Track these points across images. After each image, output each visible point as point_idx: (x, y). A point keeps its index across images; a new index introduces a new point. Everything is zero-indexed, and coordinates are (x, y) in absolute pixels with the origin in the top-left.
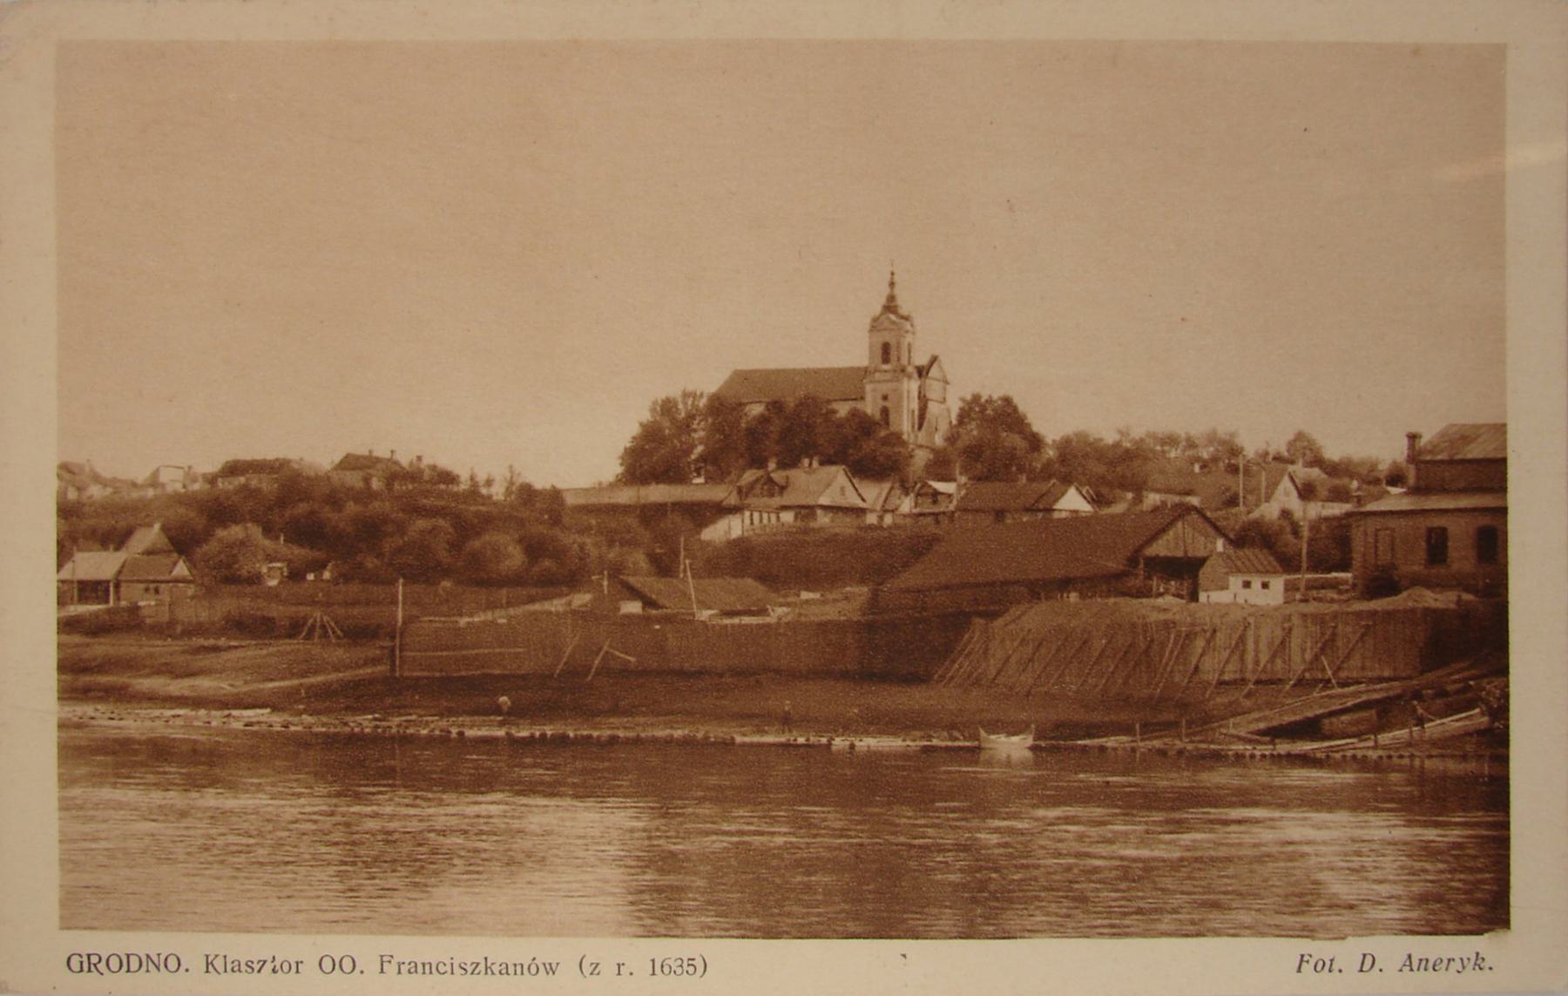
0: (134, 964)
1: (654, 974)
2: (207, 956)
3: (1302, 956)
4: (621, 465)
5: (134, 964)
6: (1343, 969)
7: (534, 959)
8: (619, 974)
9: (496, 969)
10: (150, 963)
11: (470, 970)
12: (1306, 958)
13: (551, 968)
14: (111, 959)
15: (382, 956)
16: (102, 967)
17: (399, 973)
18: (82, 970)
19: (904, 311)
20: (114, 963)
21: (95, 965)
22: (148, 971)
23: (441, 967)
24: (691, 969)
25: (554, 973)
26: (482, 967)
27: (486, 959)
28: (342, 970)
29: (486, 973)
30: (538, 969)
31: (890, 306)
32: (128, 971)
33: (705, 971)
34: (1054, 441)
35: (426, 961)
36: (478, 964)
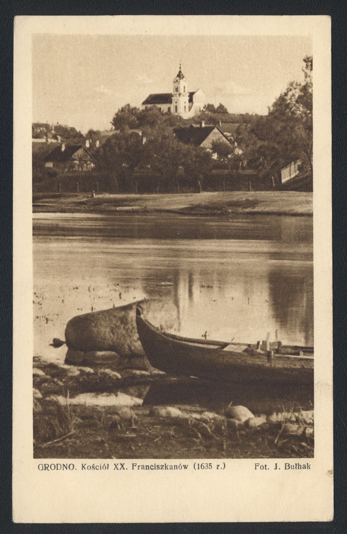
2: (82, 464)
3: (133, 464)
6: (128, 469)
7: (180, 464)
9: (169, 467)
10: (64, 467)
11: (160, 467)
12: (134, 465)
16: (49, 468)
17: (139, 469)
20: (53, 467)
22: (63, 469)
23: (97, 467)
24: (210, 467)
25: (187, 468)
26: (164, 467)
28: (70, 469)
29: (165, 469)
30: (90, 467)
33: (224, 467)
34: (85, 134)
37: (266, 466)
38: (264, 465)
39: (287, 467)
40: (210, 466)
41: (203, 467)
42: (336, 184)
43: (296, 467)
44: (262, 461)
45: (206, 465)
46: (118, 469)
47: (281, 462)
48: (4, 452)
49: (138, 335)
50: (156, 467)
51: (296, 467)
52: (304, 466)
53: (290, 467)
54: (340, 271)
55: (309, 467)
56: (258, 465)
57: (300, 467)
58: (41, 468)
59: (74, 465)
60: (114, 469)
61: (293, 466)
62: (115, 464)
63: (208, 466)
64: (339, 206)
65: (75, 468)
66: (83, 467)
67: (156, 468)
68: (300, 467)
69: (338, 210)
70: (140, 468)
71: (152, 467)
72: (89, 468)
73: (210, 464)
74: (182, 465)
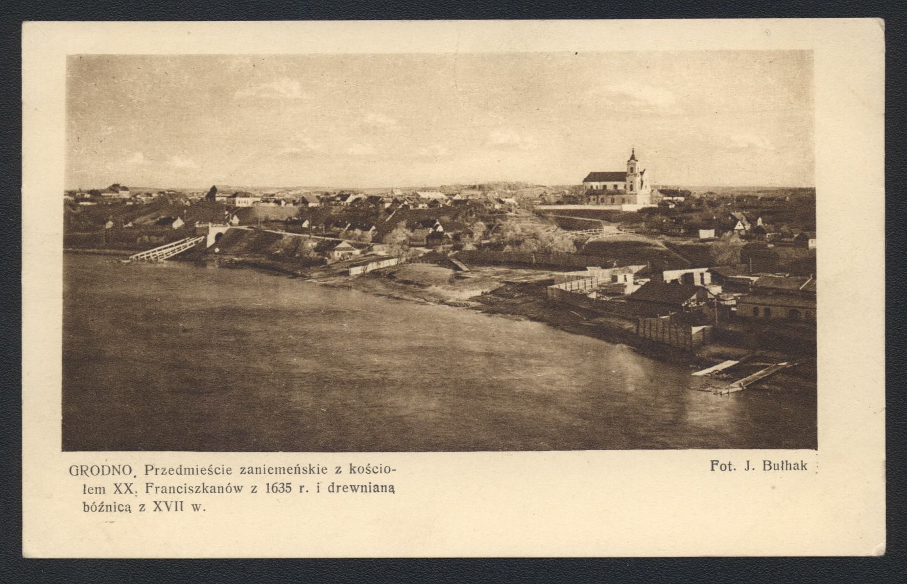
0: (106, 470)
1: (268, 492)
3: (147, 484)
5: (106, 470)
8: (318, 492)
9: (209, 489)
10: (115, 470)
13: (239, 489)
15: (147, 484)
16: (88, 472)
19: (636, 159)
20: (95, 470)
22: (113, 474)
24: (288, 489)
26: (201, 489)
27: (203, 484)
29: (204, 492)
31: (633, 157)
32: (103, 474)
36: (199, 487)
37: (730, 465)
38: (727, 463)
39: (767, 467)
40: (287, 487)
41: (275, 489)
43: (782, 467)
45: (282, 485)
47: (758, 456)
49: (469, 249)
50: (188, 490)
51: (782, 467)
53: (773, 468)
56: (151, 485)
57: (789, 466)
61: (778, 464)
62: (116, 485)
63: (285, 487)
65: (133, 473)
67: (187, 491)
68: (789, 466)
71: (290, 471)
73: (287, 484)
74: (232, 485)
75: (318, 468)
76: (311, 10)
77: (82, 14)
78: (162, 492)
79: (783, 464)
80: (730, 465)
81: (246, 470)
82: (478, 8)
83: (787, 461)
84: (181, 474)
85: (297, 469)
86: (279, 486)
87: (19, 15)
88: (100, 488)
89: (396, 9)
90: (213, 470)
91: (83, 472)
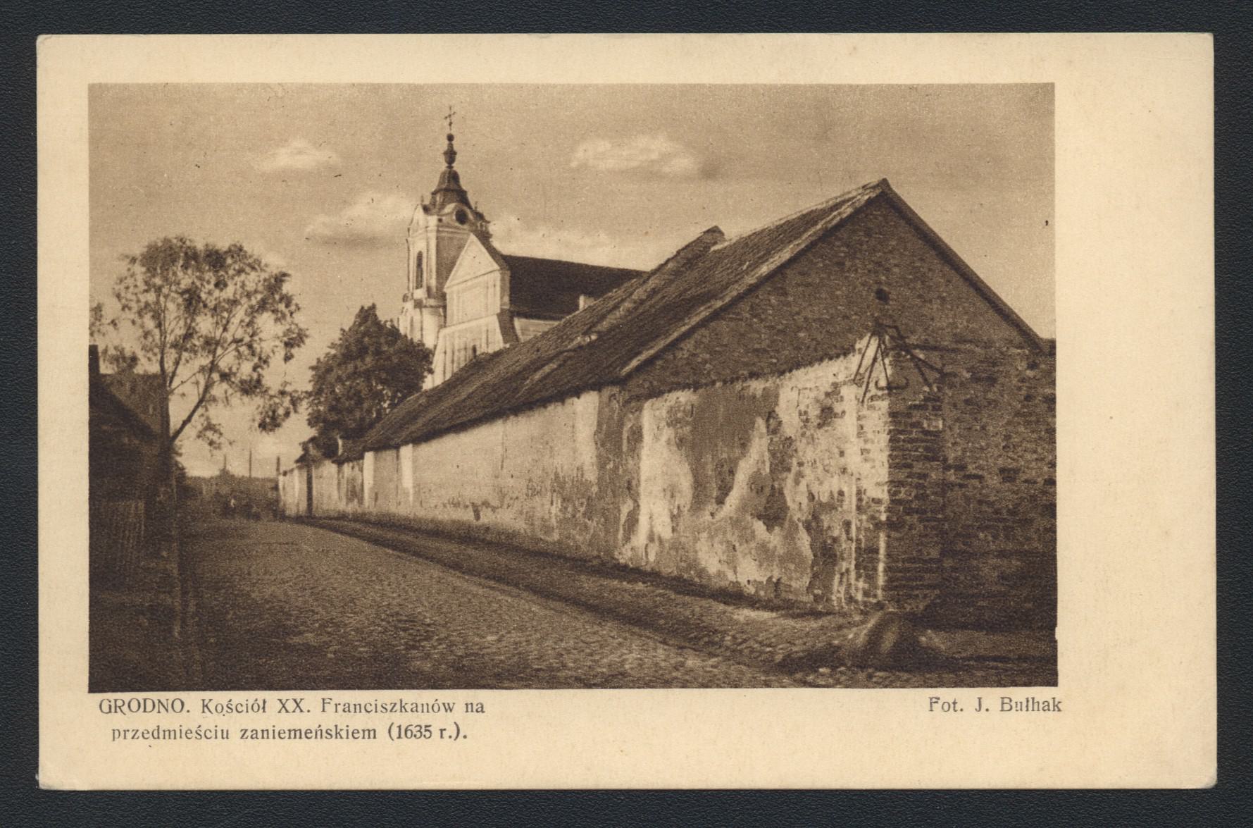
2: (203, 700)
3: (323, 700)
4: (324, 465)
9: (408, 707)
11: (389, 708)
14: (151, 708)
16: (125, 708)
18: (110, 712)
21: (120, 707)
22: (159, 712)
23: (239, 707)
24: (428, 734)
25: (451, 710)
26: (398, 707)
27: (336, 726)
29: (401, 711)
30: (216, 710)
35: (265, 729)
36: (395, 704)
37: (955, 703)
38: (951, 702)
40: (426, 731)
42: (787, 806)
43: (1027, 706)
44: (946, 694)
46: (287, 711)
48: (157, 26)
50: (379, 708)
51: (1027, 706)
52: (1046, 704)
54: (583, 813)
55: (1057, 707)
56: (329, 701)
57: (1036, 705)
58: (106, 708)
59: (183, 704)
60: (280, 712)
62: (280, 700)
63: (423, 730)
64: (734, 811)
65: (186, 708)
66: (204, 706)
68: (1036, 705)
69: (726, 810)
70: (340, 708)
72: (219, 708)
73: (426, 726)
74: (440, 702)
75: (347, 730)
76: (413, 9)
77: (98, 13)
78: (344, 711)
79: (1028, 701)
80: (955, 703)
81: (249, 734)
82: (644, 6)
83: (1033, 699)
84: (158, 738)
85: (319, 733)
86: (415, 730)
87: (10, 14)
88: (169, 731)
89: (531, 7)
90: (202, 734)
91: (118, 709)
